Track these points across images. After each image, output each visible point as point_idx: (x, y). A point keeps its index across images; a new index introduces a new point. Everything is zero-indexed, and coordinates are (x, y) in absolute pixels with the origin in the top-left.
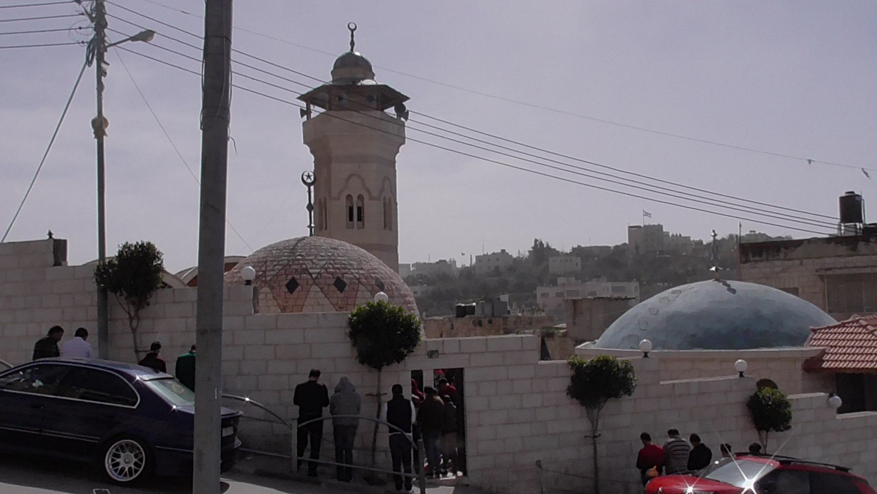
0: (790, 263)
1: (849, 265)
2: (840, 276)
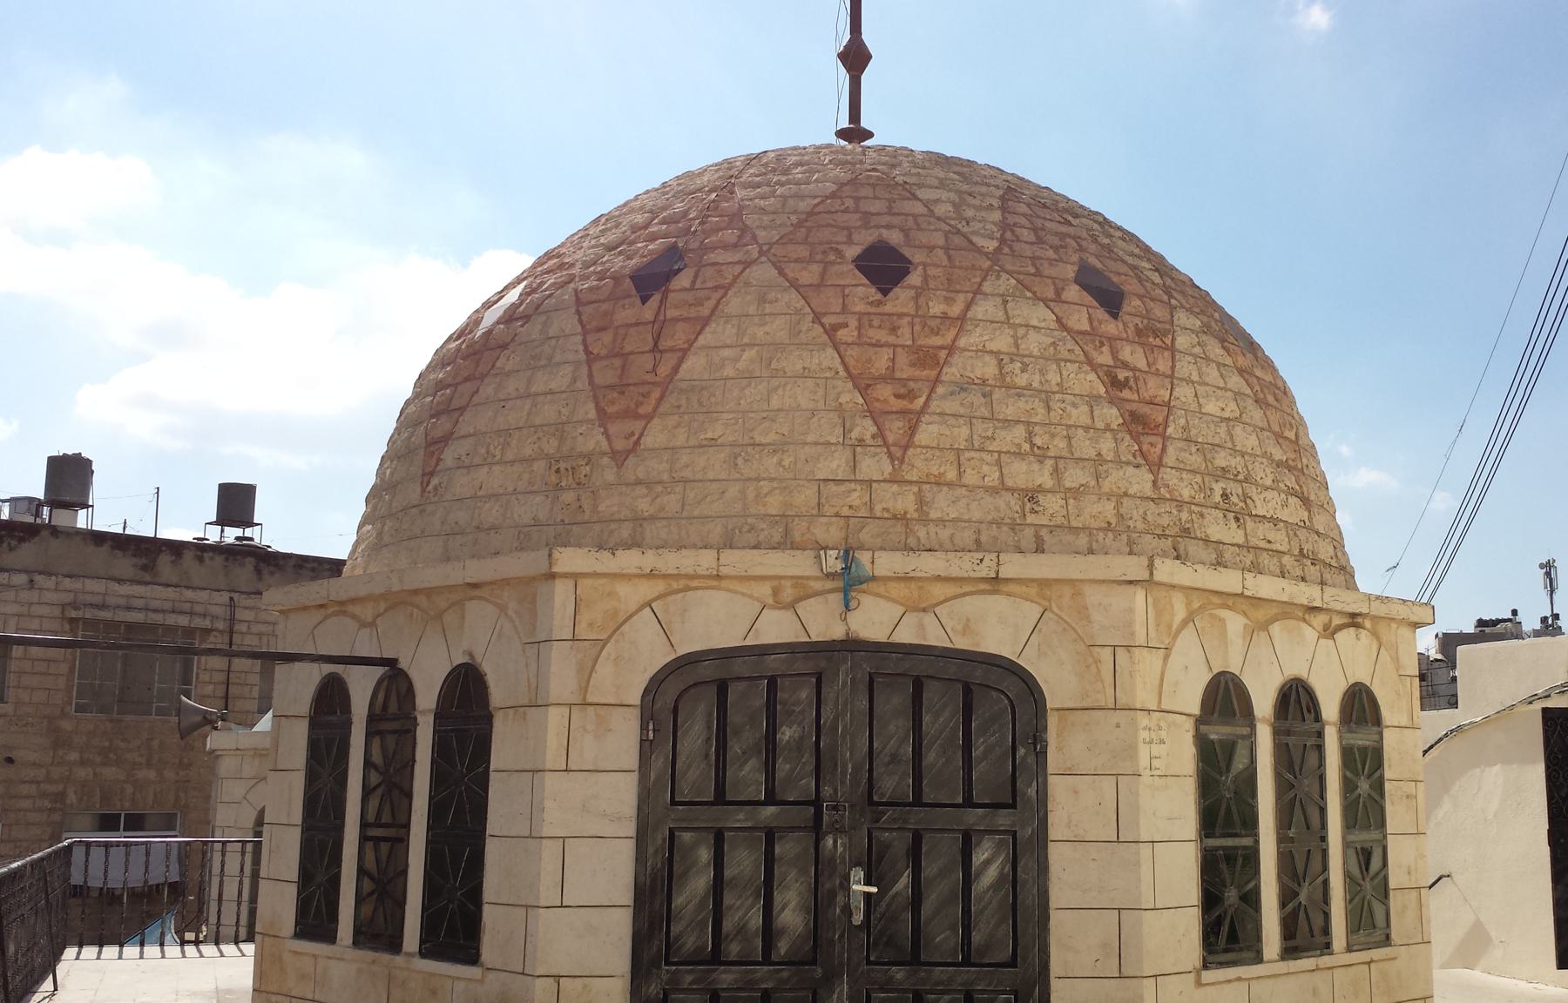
2: (111, 625)
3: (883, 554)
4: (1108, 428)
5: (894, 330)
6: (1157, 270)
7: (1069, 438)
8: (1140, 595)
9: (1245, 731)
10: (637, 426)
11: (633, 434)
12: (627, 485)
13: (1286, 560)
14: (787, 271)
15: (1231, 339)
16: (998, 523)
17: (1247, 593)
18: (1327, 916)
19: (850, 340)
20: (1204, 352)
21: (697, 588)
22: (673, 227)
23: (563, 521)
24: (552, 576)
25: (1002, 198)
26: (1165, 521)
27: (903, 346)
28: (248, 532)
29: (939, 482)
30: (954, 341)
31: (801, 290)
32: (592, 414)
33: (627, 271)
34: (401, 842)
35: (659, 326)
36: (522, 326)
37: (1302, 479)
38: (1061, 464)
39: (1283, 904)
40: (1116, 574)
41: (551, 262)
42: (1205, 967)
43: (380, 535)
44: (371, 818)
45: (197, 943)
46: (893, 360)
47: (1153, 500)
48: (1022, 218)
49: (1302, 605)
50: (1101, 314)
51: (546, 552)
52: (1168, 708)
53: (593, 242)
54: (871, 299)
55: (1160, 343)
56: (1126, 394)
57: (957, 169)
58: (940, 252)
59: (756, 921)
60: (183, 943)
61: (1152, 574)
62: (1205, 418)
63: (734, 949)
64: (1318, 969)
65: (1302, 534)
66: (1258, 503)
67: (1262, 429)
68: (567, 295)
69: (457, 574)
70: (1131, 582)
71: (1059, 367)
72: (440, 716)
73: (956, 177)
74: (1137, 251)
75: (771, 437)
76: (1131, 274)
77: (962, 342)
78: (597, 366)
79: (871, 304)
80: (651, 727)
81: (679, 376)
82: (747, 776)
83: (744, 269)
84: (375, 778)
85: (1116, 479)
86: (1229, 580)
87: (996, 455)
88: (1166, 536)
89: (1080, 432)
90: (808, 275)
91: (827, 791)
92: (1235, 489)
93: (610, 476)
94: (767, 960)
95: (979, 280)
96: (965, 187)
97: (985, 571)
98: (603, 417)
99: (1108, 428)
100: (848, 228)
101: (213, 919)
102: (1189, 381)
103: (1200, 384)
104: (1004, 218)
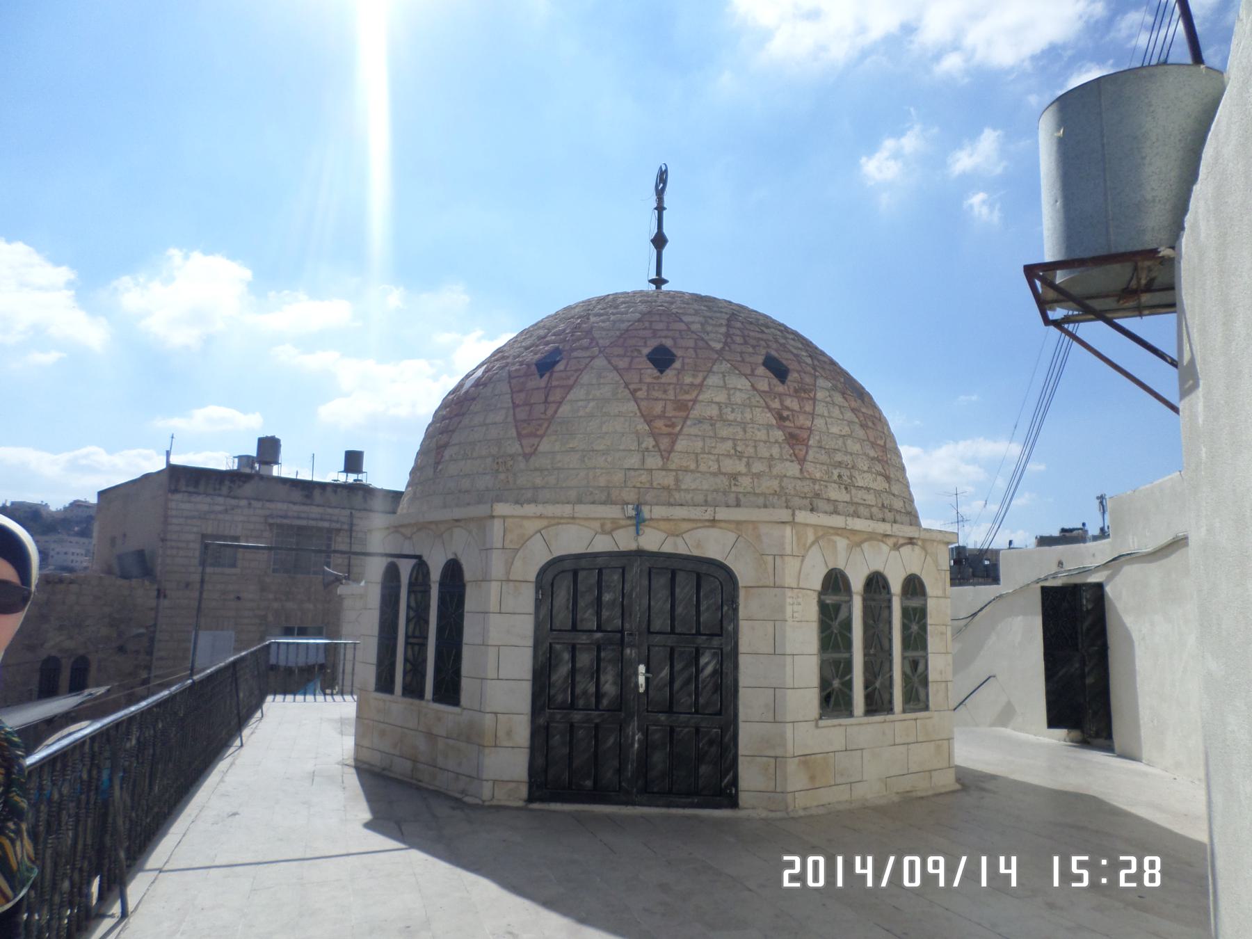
0: (233, 502)
1: (303, 515)
2: (290, 527)
3: (656, 507)
4: (776, 442)
5: (665, 391)
6: (810, 356)
7: (755, 447)
8: (788, 529)
9: (847, 598)
10: (535, 441)
11: (533, 445)
12: (531, 471)
13: (874, 510)
14: (612, 361)
15: (849, 392)
16: (716, 491)
17: (848, 528)
18: (891, 695)
19: (643, 397)
20: (832, 401)
21: (563, 524)
22: (558, 337)
23: (499, 488)
24: (493, 517)
25: (729, 320)
26: (806, 489)
27: (670, 400)
28: (360, 477)
29: (686, 470)
30: (696, 397)
31: (619, 371)
32: (515, 434)
33: (534, 361)
34: (423, 646)
35: (548, 389)
36: (483, 389)
37: (886, 466)
38: (751, 460)
39: (866, 687)
40: (776, 518)
41: (499, 354)
42: (821, 718)
43: (415, 493)
44: (410, 633)
45: (332, 694)
46: (665, 408)
47: (800, 479)
48: (738, 330)
49: (881, 534)
50: (775, 381)
51: (490, 505)
52: (804, 587)
53: (519, 345)
54: (654, 376)
55: (807, 396)
56: (787, 423)
57: (706, 304)
58: (691, 351)
59: (592, 689)
60: (325, 694)
61: (794, 519)
62: (830, 435)
63: (581, 703)
64: (885, 721)
65: (884, 496)
66: (858, 479)
67: (864, 441)
68: (504, 374)
69: (448, 515)
70: (783, 523)
71: (751, 409)
72: (442, 584)
73: (705, 308)
74: (800, 346)
75: (602, 447)
76: (795, 359)
77: (701, 398)
78: (518, 410)
79: (655, 378)
80: (540, 592)
81: (557, 416)
82: (588, 619)
83: (592, 360)
84: (412, 614)
85: (779, 468)
86: (838, 521)
87: (717, 456)
88: (806, 498)
89: (762, 444)
90: (622, 364)
91: (627, 626)
92: (845, 473)
93: (522, 465)
94: (597, 709)
95: (710, 365)
96: (708, 314)
97: (708, 516)
98: (520, 436)
99: (776, 442)
100: (645, 338)
101: (340, 682)
102: (823, 416)
103: (828, 417)
104: (728, 330)
